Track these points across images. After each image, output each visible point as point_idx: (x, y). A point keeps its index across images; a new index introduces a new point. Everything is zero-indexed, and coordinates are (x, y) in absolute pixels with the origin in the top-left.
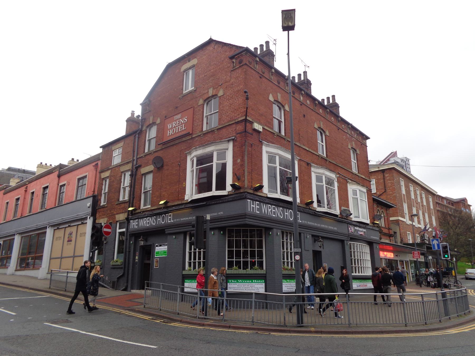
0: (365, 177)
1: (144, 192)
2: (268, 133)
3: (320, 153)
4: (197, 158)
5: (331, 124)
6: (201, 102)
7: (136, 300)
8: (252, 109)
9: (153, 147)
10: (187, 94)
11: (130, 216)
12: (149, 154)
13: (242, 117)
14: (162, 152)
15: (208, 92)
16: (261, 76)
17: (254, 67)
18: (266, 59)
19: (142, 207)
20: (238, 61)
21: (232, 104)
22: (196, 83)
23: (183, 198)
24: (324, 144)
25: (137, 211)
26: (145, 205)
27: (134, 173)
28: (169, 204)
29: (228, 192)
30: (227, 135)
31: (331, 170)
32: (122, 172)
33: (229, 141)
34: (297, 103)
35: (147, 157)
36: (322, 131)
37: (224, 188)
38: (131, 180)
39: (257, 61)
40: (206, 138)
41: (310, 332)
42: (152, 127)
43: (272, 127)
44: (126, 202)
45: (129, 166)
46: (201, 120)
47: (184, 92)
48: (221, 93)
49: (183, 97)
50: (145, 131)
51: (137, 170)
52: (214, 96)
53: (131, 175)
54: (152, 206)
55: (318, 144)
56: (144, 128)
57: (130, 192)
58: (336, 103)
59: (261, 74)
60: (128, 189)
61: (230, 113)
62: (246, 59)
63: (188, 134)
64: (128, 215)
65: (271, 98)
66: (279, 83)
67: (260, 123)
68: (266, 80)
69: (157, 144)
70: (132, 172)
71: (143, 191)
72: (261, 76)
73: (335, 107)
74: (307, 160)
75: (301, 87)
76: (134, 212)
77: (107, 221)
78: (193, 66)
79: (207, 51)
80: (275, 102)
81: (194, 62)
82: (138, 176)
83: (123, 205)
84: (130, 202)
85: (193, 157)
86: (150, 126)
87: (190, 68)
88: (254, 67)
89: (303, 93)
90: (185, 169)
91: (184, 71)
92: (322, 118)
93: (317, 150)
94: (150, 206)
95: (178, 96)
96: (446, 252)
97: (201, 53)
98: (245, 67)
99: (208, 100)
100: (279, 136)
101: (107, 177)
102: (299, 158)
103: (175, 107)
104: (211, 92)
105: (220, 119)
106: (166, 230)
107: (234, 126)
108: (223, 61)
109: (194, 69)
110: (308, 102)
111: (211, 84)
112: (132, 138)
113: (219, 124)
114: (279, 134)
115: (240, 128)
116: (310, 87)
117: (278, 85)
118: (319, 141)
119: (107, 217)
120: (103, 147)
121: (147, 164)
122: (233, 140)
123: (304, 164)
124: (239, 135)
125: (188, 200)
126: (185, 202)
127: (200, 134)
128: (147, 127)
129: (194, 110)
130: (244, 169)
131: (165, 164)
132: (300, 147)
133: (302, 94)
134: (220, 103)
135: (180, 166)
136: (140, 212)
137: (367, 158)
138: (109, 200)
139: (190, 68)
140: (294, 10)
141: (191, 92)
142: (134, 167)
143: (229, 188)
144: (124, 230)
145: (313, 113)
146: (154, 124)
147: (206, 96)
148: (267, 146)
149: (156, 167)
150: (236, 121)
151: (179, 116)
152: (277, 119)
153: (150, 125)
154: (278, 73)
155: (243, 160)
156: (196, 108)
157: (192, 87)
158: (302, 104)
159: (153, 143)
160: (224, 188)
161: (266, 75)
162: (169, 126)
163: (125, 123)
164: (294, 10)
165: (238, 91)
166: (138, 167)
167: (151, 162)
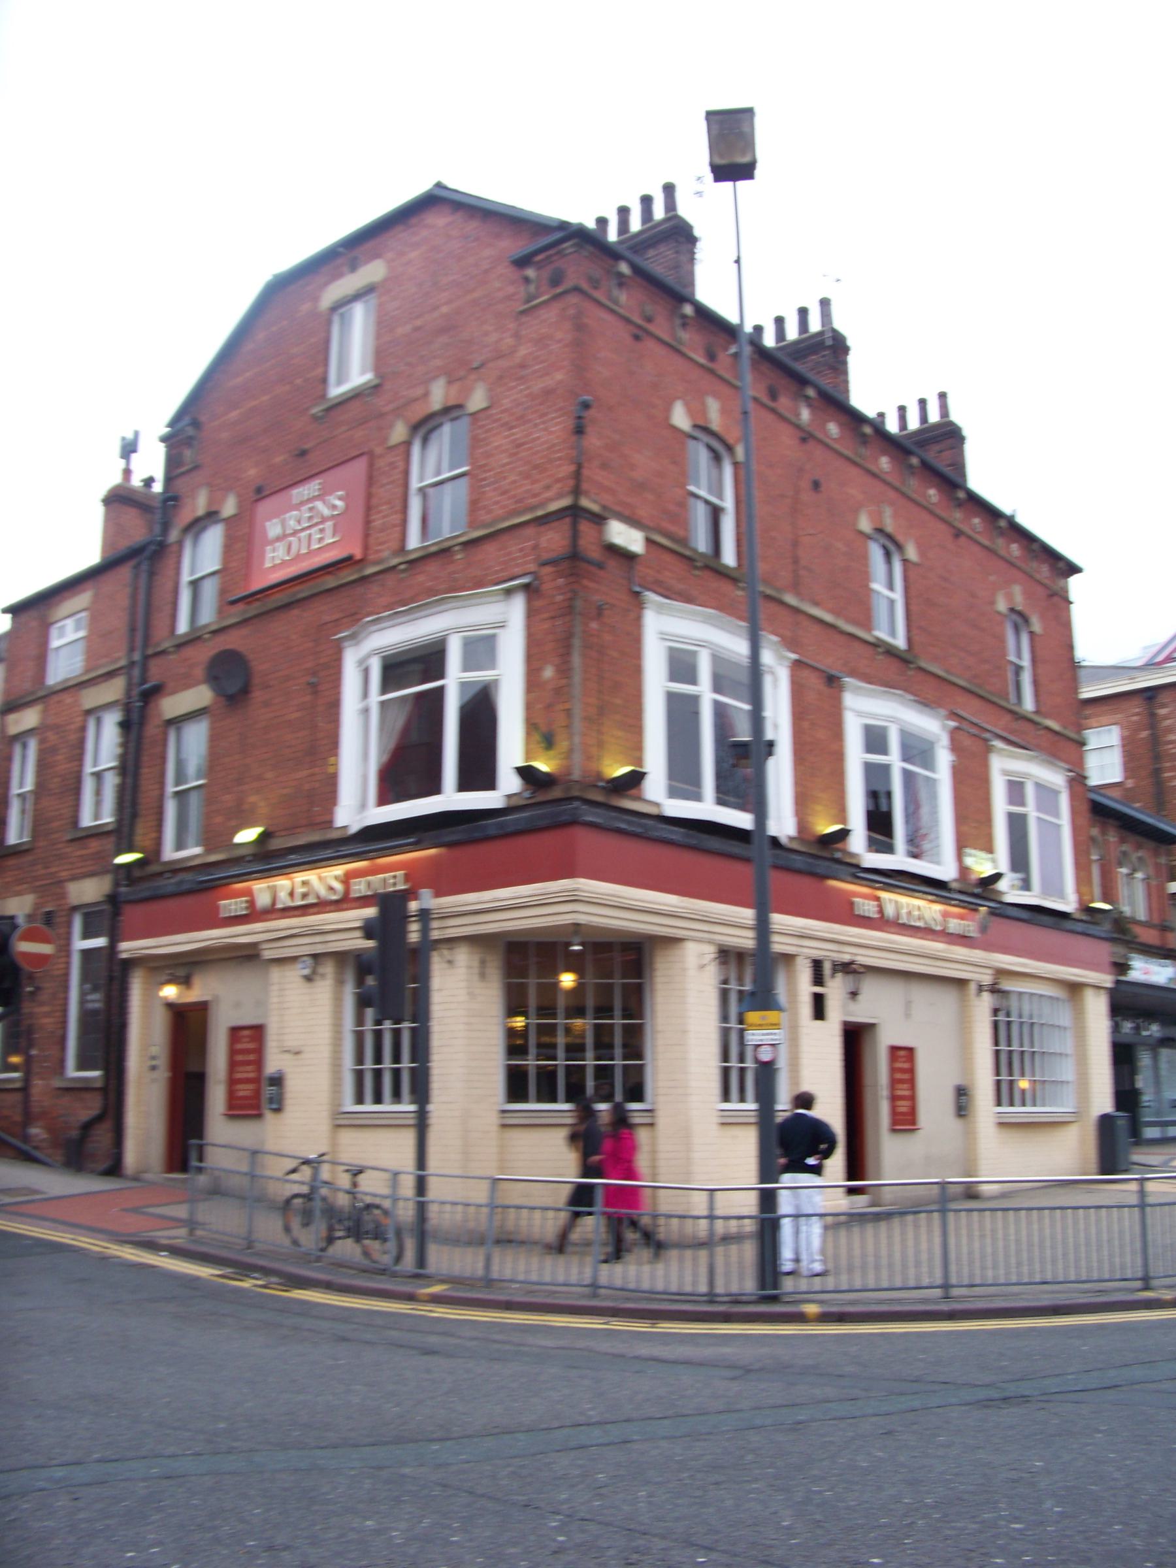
0: (1065, 727)
1: (177, 794)
2: (667, 557)
3: (882, 634)
4: (385, 659)
5: (925, 516)
6: (399, 432)
7: (151, 1210)
8: (604, 466)
9: (207, 616)
10: (340, 400)
11: (123, 889)
12: (194, 639)
13: (560, 496)
14: (245, 631)
15: (426, 395)
16: (640, 333)
17: (610, 298)
18: (658, 263)
19: (170, 854)
20: (546, 273)
21: (524, 444)
22: (381, 357)
23: (327, 818)
24: (898, 596)
25: (154, 868)
26: (180, 845)
27: (135, 716)
28: (276, 844)
29: (509, 796)
30: (502, 570)
31: (926, 703)
32: (89, 712)
33: (509, 592)
34: (787, 439)
35: (188, 652)
36: (892, 545)
37: (489, 783)
38: (124, 745)
39: (620, 275)
40: (421, 578)
41: (801, 1318)
42: (204, 529)
43: (681, 533)
44: (108, 833)
45: (114, 690)
46: (398, 507)
47: (336, 391)
48: (477, 400)
49: (329, 410)
50: (174, 548)
51: (143, 709)
52: (451, 411)
53: (125, 726)
54: (209, 850)
55: (874, 597)
56: (174, 535)
57: (121, 791)
58: (951, 424)
59: (639, 327)
60: (111, 782)
61: (514, 482)
62: (577, 266)
63: (347, 562)
64: (117, 884)
65: (680, 418)
66: (712, 357)
67: (632, 521)
68: (660, 351)
69: (228, 602)
70: (127, 709)
71: (171, 788)
72: (640, 333)
73: (950, 441)
74: (828, 663)
75: (800, 367)
76: (137, 873)
77: (37, 906)
78: (370, 290)
79: (425, 233)
80: (697, 434)
81: (373, 271)
82: (151, 730)
83: (94, 845)
84: (121, 834)
85: (368, 656)
86: (197, 526)
87: (356, 297)
88: (610, 298)
89: (811, 392)
90: (334, 706)
91: (334, 309)
92: (891, 494)
93: (867, 624)
94: (197, 850)
95: (308, 409)
96: (579, 1012)
97: (398, 238)
98: (574, 299)
99: (425, 427)
100: (712, 565)
101: (30, 732)
102: (794, 656)
103: (297, 452)
104: (438, 395)
105: (474, 505)
106: (264, 946)
107: (529, 531)
108: (486, 271)
109: (373, 299)
110: (833, 428)
111: (438, 362)
112: (125, 572)
113: (473, 525)
114: (712, 564)
115: (554, 540)
116: (845, 363)
117: (710, 365)
118: (878, 586)
119: (34, 890)
120: (16, 610)
121: (187, 683)
122: (526, 587)
123: (814, 682)
124: (548, 570)
125: (345, 827)
126: (334, 835)
127: (394, 562)
128: (187, 529)
129: (371, 465)
130: (567, 706)
131: (256, 681)
132: (796, 611)
133: (807, 398)
134: (476, 442)
135: (314, 688)
136: (160, 874)
137: (1070, 647)
138: (39, 825)
139: (356, 297)
140: (749, 112)
141: (356, 395)
142: (136, 692)
143: (509, 783)
144: (100, 942)
145: (854, 472)
146: (211, 516)
147: (418, 412)
148: (660, 609)
149: (218, 690)
150: (540, 513)
151: (311, 489)
152: (707, 502)
153: (197, 520)
154: (708, 319)
155: (564, 671)
156: (381, 456)
157: (363, 372)
158: (806, 437)
159: (210, 591)
160: (489, 783)
161: (660, 327)
162: (273, 529)
163: (99, 511)
164: (749, 112)
165: (548, 392)
166: (151, 694)
167: (199, 672)
